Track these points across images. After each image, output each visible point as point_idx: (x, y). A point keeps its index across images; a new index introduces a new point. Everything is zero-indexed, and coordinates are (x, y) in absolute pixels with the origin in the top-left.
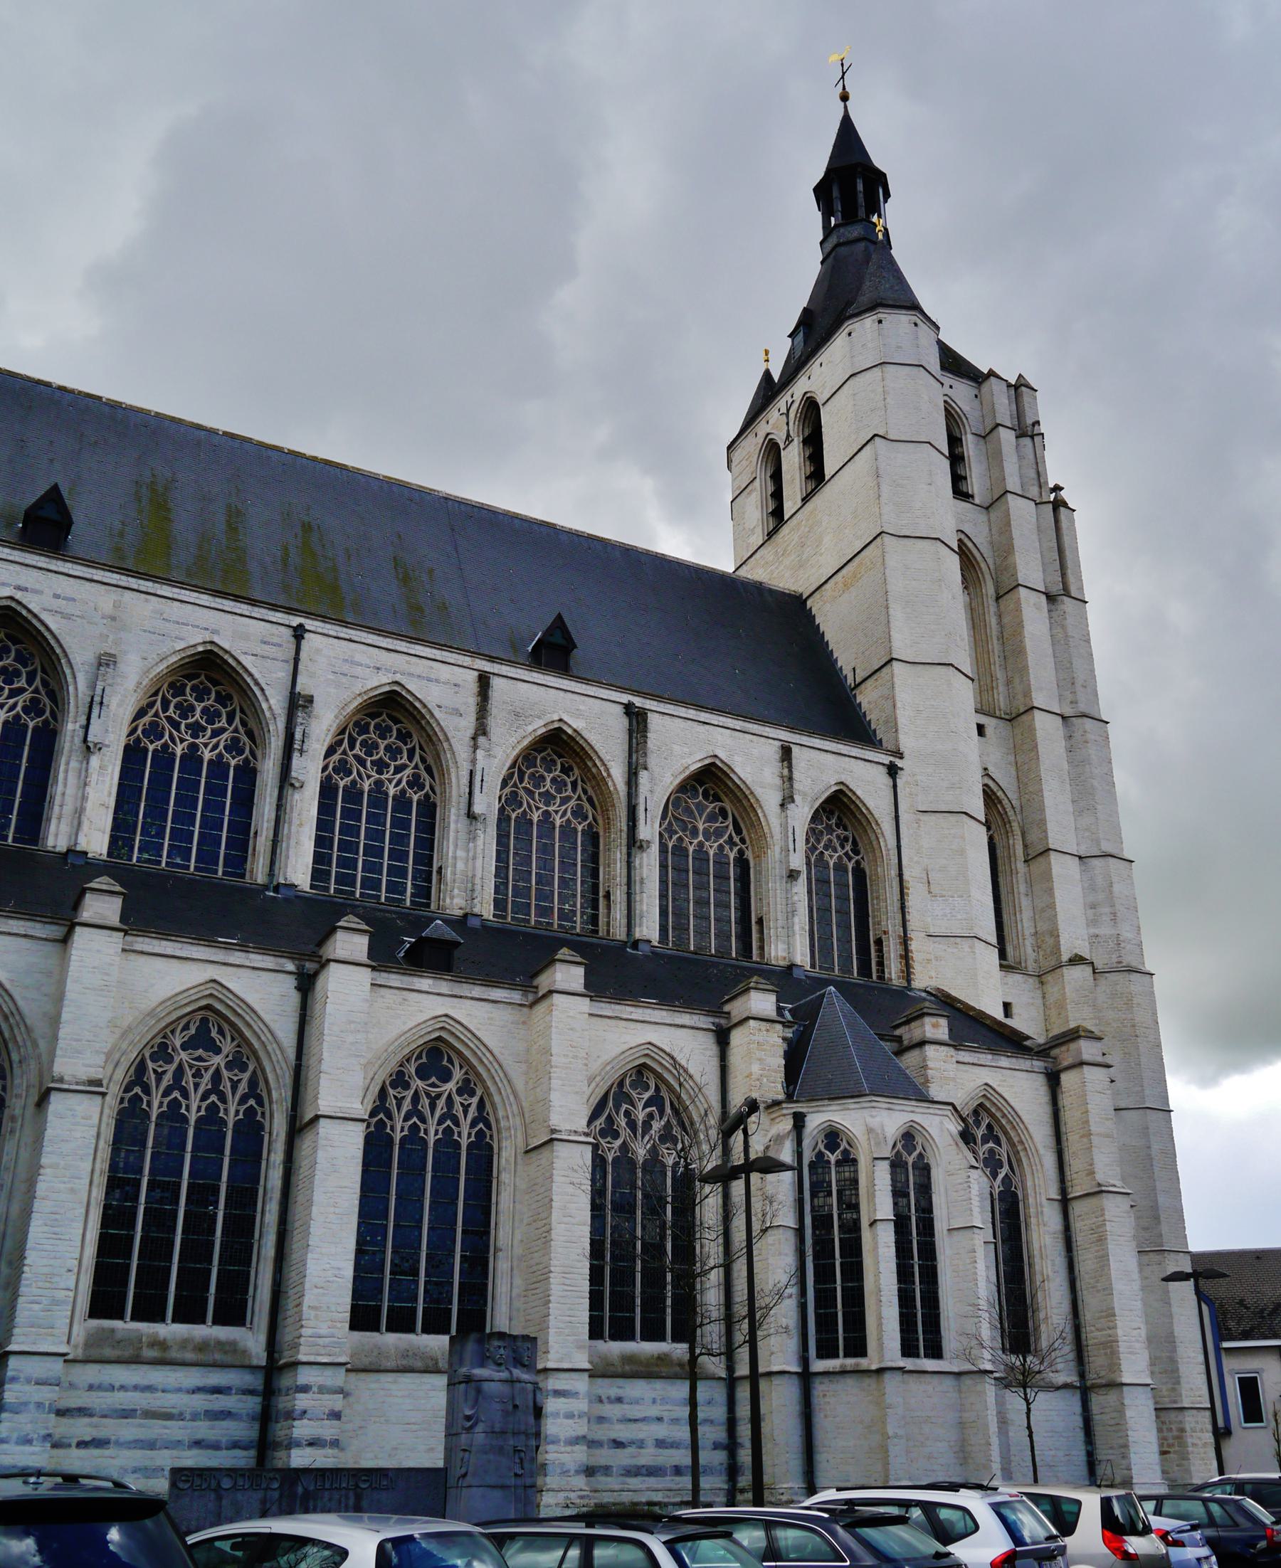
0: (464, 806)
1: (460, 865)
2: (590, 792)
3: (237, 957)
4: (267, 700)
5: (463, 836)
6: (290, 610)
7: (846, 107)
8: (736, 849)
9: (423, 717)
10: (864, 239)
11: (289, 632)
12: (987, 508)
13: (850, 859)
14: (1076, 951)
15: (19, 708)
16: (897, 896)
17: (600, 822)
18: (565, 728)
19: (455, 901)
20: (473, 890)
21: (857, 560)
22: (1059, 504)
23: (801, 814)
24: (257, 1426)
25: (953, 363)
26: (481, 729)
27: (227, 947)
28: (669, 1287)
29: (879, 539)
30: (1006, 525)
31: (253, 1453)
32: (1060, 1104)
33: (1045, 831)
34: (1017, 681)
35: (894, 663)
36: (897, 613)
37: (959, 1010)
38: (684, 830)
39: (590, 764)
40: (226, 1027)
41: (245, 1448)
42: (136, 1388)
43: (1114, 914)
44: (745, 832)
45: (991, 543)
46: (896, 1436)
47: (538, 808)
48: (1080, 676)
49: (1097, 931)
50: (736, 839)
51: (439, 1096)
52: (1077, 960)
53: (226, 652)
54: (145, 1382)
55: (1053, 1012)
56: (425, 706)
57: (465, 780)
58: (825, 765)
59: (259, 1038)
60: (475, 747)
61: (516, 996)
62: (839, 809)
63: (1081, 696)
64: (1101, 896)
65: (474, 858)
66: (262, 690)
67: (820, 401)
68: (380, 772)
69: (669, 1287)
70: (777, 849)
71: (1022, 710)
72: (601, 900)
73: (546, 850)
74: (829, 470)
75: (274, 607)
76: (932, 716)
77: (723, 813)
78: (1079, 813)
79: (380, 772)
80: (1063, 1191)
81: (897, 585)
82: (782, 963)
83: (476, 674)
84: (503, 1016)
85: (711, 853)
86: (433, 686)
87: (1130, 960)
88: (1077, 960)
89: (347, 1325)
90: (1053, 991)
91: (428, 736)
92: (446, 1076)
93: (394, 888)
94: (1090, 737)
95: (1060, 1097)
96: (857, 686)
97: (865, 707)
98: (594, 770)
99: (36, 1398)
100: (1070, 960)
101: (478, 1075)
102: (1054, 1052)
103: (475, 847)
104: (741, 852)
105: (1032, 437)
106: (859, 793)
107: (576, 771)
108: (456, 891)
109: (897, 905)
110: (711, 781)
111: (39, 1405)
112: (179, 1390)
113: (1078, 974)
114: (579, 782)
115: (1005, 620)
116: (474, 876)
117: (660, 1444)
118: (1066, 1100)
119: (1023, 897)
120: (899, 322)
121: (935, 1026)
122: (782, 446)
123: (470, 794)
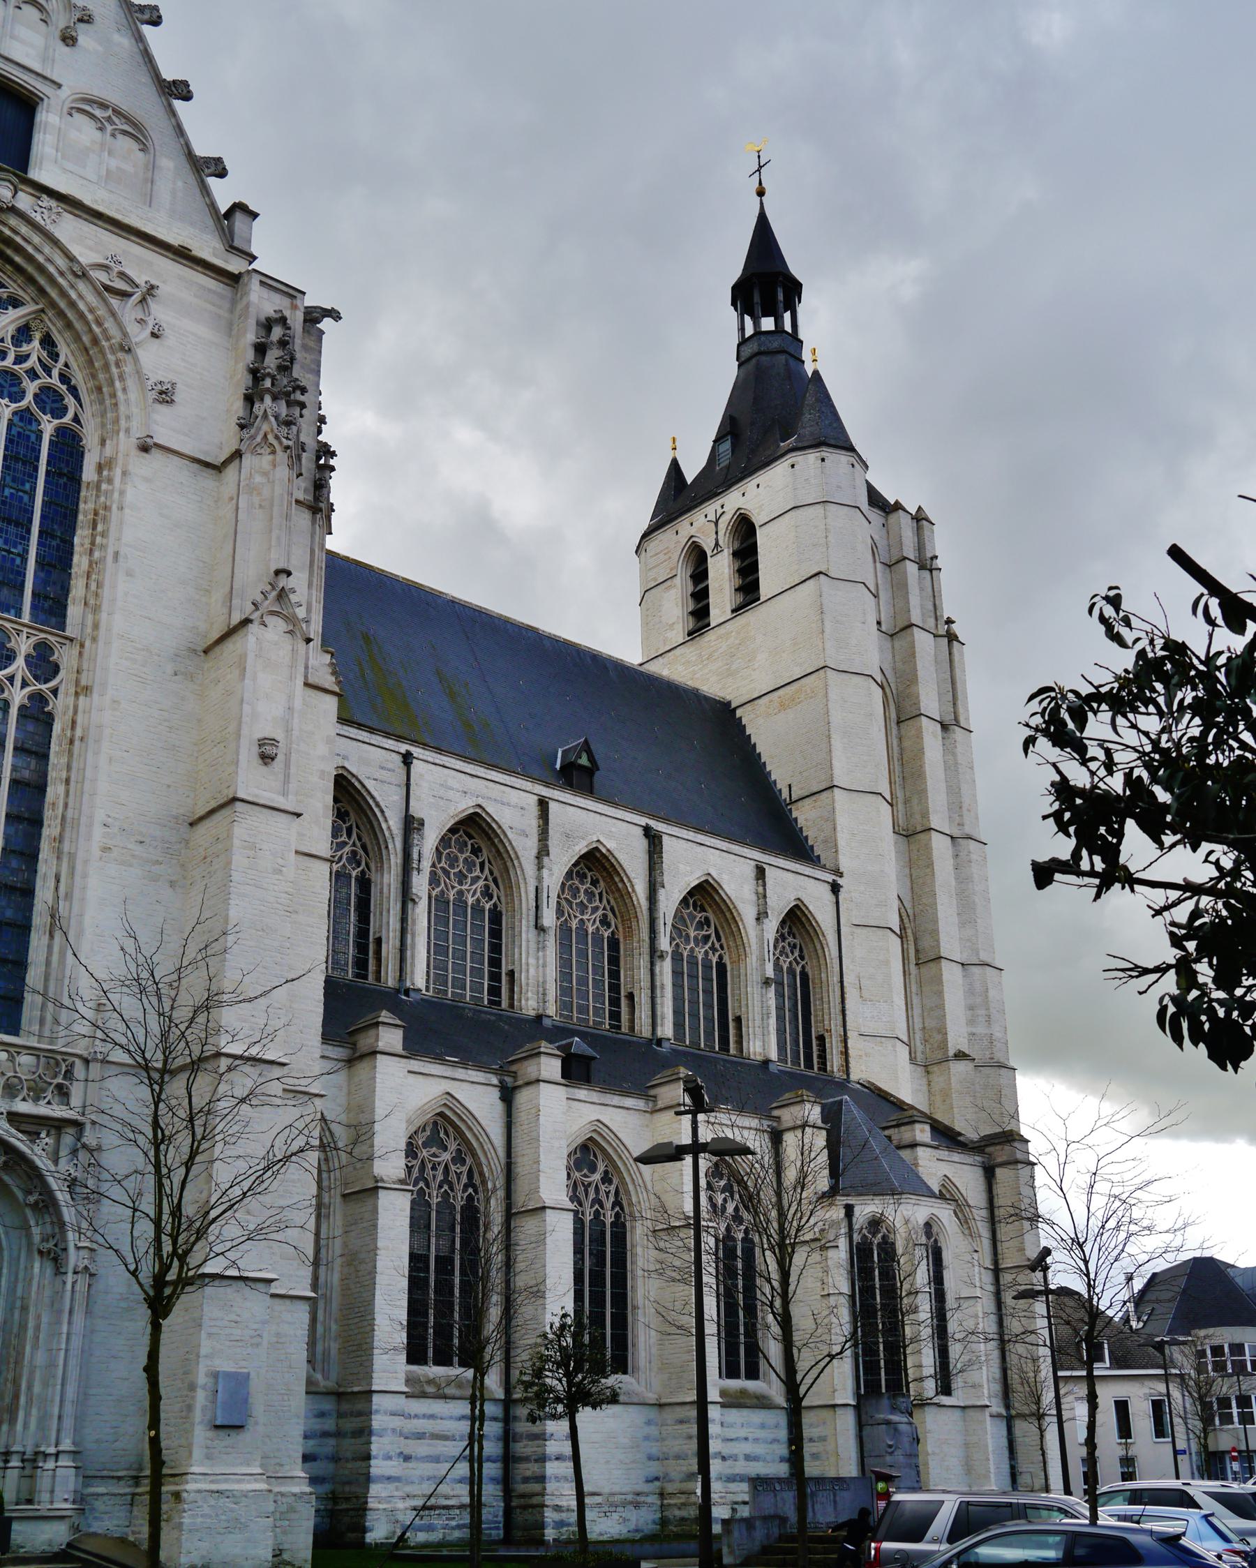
0: (532, 918)
1: (532, 971)
2: (612, 902)
3: (460, 1073)
4: (386, 821)
5: (533, 945)
6: (399, 738)
7: (762, 204)
8: (717, 954)
9: (497, 836)
10: (783, 352)
11: (399, 759)
12: (891, 636)
13: (798, 963)
14: (959, 1047)
15: (344, 860)
16: (838, 1000)
17: (621, 929)
18: (601, 847)
19: (530, 1002)
20: (544, 994)
21: (796, 685)
22: (952, 637)
23: (772, 926)
24: (501, 1444)
25: (875, 499)
26: (543, 852)
27: (454, 1065)
28: (742, 1337)
29: (821, 672)
30: (911, 654)
31: (499, 1465)
32: (995, 1192)
33: (938, 941)
34: (915, 801)
35: (836, 790)
36: (837, 743)
37: (892, 1103)
38: (680, 937)
39: (617, 879)
40: (451, 1130)
41: (494, 1462)
42: (424, 1416)
43: (989, 1016)
44: (723, 940)
45: (894, 669)
46: (934, 1454)
47: (453, 887)
48: (966, 801)
49: (974, 1030)
50: (717, 946)
51: (590, 1184)
52: (961, 1056)
53: (354, 776)
54: (430, 1412)
55: (938, 1099)
56: (500, 827)
57: (532, 896)
58: (790, 883)
59: (478, 1139)
60: (540, 867)
61: (640, 1104)
62: (797, 921)
63: (967, 820)
64: (979, 1000)
65: (544, 966)
66: (382, 812)
67: (757, 520)
68: (461, 883)
69: (742, 1337)
70: (754, 958)
71: (919, 829)
72: (623, 999)
73: (583, 954)
74: (765, 590)
75: (387, 735)
76: (859, 833)
77: (708, 921)
78: (962, 925)
79: (461, 883)
80: (996, 1262)
81: (836, 717)
82: (759, 1058)
83: (536, 798)
84: (633, 1120)
85: (700, 958)
86: (505, 808)
87: (999, 1056)
88: (961, 1056)
89: (403, 1357)
90: (938, 1080)
91: (498, 851)
92: (593, 1169)
93: (477, 987)
94: (974, 857)
95: (994, 1187)
96: (791, 803)
97: (801, 823)
98: (620, 885)
99: (391, 1426)
100: (956, 1055)
101: (616, 1167)
102: (988, 1150)
103: (544, 956)
104: (721, 957)
105: (931, 571)
106: (811, 908)
107: (602, 883)
108: (530, 994)
109: (839, 1007)
110: (704, 895)
111: (394, 1430)
112: (451, 1418)
113: (959, 1068)
114: (355, 830)
115: (906, 744)
116: (544, 982)
117: (748, 1458)
118: (1000, 1190)
119: (914, 996)
120: (839, 460)
121: (922, 1131)
122: (709, 553)
123: (537, 907)
